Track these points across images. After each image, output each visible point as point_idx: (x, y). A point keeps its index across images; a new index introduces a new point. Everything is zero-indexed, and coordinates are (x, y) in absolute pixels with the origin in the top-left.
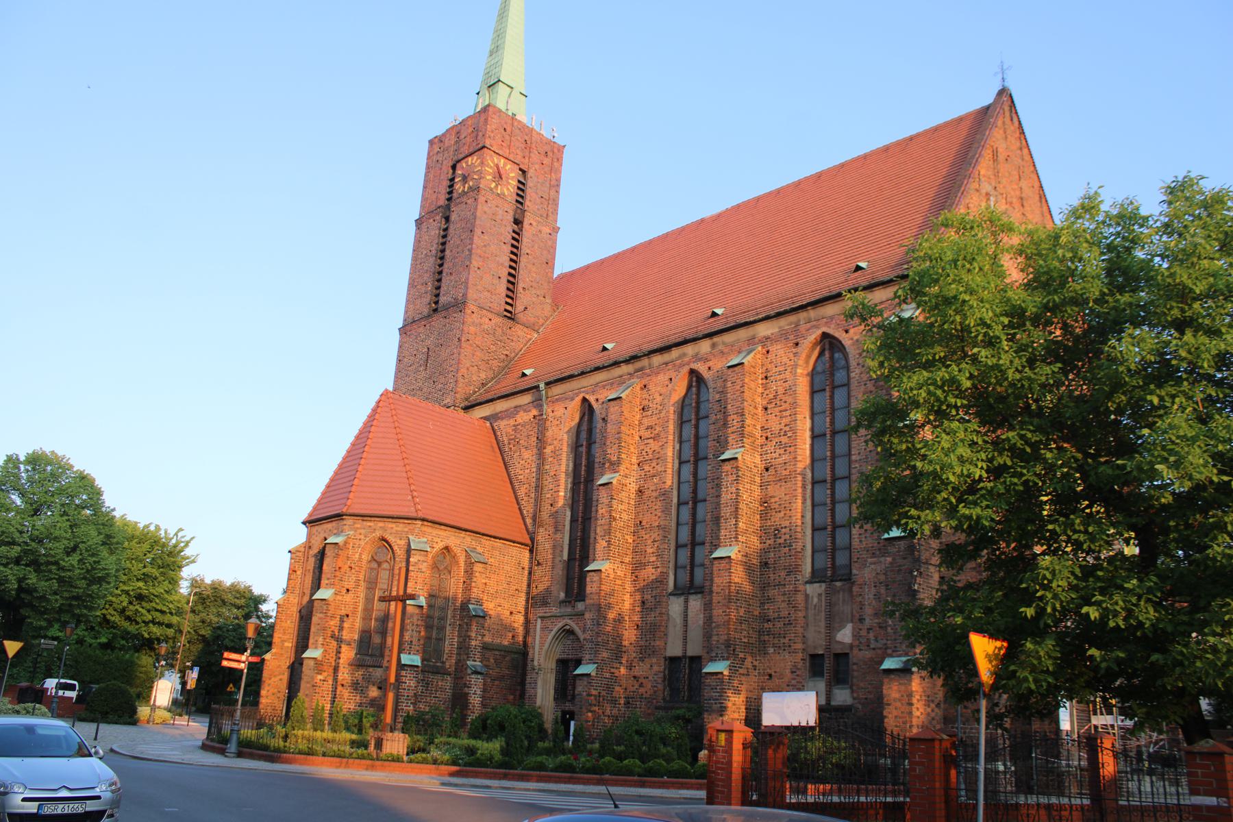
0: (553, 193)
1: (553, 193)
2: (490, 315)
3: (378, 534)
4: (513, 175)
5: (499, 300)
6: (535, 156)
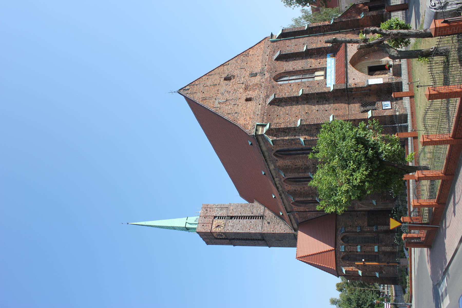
2: (263, 224)
4: (216, 222)
5: (259, 221)
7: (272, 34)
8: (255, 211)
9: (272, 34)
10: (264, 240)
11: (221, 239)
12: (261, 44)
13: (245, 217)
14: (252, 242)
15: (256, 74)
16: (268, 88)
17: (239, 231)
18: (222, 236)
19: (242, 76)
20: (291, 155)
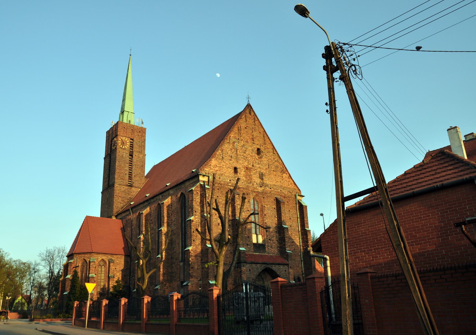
0: (143, 144)
1: (143, 144)
2: (123, 186)
3: (83, 258)
4: (128, 141)
5: (126, 181)
6: (136, 134)
7: (303, 196)
8: (137, 178)
9: (303, 196)
10: (109, 186)
11: (111, 145)
12: (294, 186)
13: (131, 169)
14: (107, 176)
15: (262, 179)
16: (247, 189)
17: (117, 162)
18: (114, 146)
19: (261, 166)
20: (182, 209)
